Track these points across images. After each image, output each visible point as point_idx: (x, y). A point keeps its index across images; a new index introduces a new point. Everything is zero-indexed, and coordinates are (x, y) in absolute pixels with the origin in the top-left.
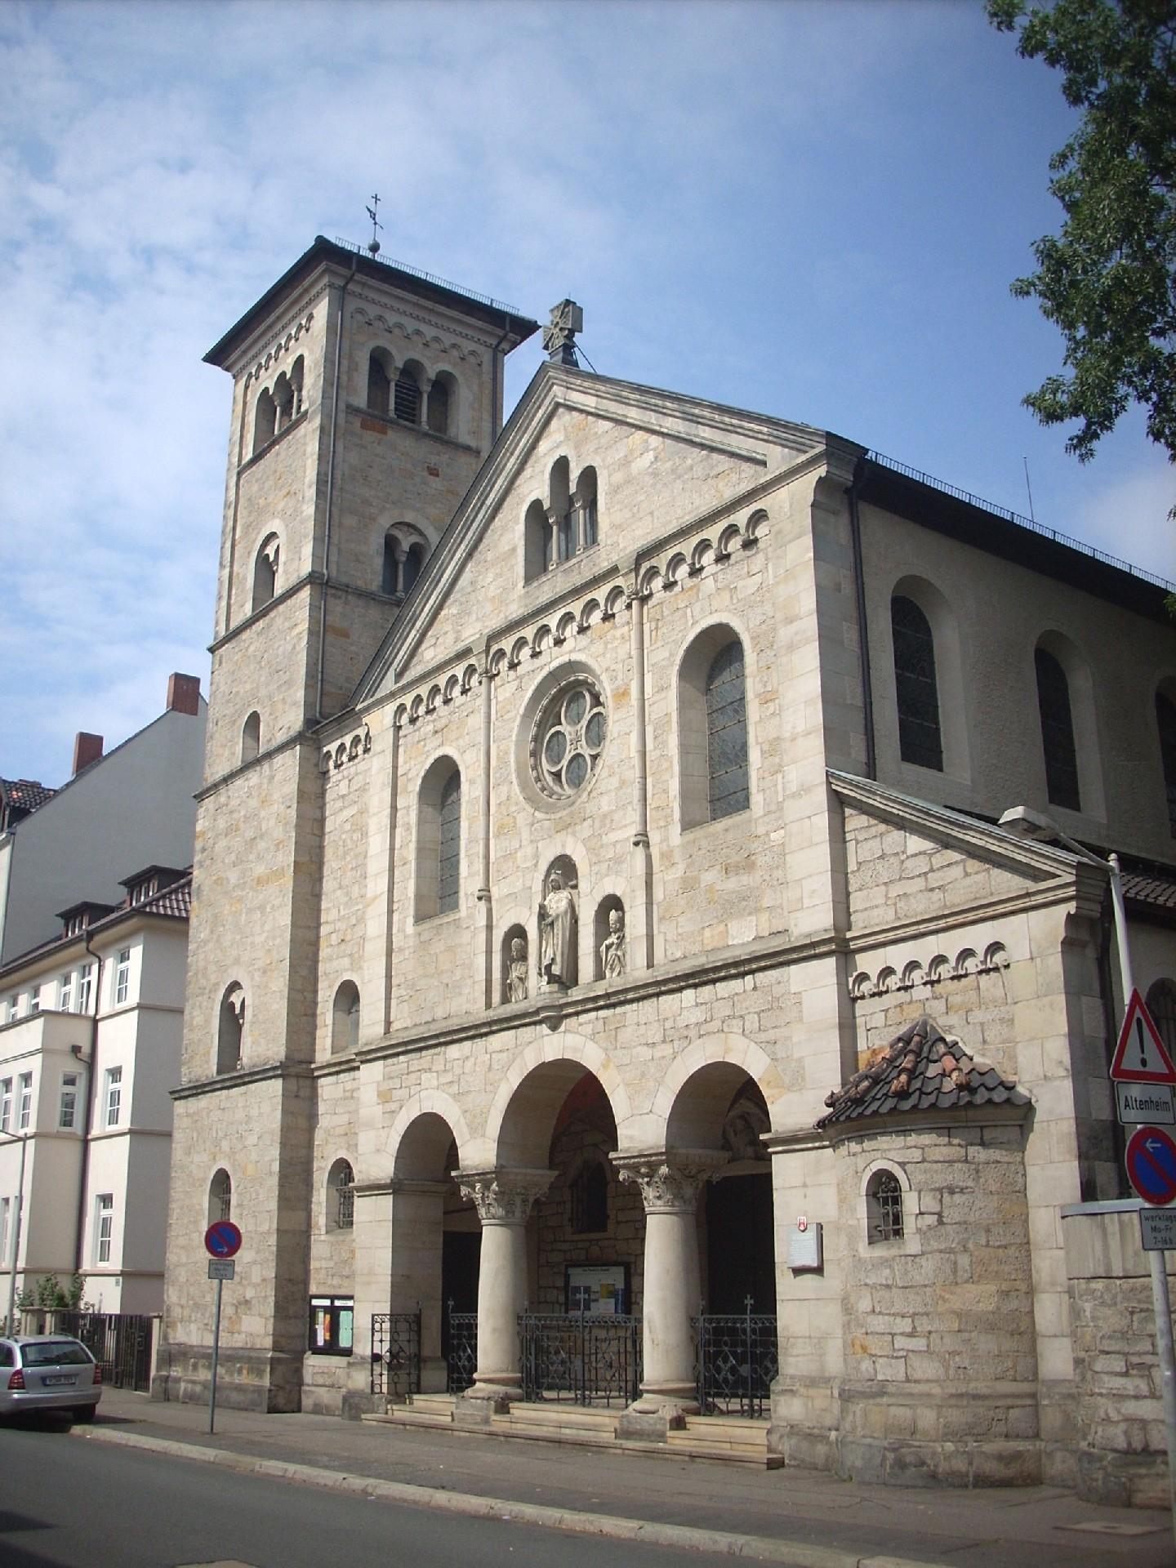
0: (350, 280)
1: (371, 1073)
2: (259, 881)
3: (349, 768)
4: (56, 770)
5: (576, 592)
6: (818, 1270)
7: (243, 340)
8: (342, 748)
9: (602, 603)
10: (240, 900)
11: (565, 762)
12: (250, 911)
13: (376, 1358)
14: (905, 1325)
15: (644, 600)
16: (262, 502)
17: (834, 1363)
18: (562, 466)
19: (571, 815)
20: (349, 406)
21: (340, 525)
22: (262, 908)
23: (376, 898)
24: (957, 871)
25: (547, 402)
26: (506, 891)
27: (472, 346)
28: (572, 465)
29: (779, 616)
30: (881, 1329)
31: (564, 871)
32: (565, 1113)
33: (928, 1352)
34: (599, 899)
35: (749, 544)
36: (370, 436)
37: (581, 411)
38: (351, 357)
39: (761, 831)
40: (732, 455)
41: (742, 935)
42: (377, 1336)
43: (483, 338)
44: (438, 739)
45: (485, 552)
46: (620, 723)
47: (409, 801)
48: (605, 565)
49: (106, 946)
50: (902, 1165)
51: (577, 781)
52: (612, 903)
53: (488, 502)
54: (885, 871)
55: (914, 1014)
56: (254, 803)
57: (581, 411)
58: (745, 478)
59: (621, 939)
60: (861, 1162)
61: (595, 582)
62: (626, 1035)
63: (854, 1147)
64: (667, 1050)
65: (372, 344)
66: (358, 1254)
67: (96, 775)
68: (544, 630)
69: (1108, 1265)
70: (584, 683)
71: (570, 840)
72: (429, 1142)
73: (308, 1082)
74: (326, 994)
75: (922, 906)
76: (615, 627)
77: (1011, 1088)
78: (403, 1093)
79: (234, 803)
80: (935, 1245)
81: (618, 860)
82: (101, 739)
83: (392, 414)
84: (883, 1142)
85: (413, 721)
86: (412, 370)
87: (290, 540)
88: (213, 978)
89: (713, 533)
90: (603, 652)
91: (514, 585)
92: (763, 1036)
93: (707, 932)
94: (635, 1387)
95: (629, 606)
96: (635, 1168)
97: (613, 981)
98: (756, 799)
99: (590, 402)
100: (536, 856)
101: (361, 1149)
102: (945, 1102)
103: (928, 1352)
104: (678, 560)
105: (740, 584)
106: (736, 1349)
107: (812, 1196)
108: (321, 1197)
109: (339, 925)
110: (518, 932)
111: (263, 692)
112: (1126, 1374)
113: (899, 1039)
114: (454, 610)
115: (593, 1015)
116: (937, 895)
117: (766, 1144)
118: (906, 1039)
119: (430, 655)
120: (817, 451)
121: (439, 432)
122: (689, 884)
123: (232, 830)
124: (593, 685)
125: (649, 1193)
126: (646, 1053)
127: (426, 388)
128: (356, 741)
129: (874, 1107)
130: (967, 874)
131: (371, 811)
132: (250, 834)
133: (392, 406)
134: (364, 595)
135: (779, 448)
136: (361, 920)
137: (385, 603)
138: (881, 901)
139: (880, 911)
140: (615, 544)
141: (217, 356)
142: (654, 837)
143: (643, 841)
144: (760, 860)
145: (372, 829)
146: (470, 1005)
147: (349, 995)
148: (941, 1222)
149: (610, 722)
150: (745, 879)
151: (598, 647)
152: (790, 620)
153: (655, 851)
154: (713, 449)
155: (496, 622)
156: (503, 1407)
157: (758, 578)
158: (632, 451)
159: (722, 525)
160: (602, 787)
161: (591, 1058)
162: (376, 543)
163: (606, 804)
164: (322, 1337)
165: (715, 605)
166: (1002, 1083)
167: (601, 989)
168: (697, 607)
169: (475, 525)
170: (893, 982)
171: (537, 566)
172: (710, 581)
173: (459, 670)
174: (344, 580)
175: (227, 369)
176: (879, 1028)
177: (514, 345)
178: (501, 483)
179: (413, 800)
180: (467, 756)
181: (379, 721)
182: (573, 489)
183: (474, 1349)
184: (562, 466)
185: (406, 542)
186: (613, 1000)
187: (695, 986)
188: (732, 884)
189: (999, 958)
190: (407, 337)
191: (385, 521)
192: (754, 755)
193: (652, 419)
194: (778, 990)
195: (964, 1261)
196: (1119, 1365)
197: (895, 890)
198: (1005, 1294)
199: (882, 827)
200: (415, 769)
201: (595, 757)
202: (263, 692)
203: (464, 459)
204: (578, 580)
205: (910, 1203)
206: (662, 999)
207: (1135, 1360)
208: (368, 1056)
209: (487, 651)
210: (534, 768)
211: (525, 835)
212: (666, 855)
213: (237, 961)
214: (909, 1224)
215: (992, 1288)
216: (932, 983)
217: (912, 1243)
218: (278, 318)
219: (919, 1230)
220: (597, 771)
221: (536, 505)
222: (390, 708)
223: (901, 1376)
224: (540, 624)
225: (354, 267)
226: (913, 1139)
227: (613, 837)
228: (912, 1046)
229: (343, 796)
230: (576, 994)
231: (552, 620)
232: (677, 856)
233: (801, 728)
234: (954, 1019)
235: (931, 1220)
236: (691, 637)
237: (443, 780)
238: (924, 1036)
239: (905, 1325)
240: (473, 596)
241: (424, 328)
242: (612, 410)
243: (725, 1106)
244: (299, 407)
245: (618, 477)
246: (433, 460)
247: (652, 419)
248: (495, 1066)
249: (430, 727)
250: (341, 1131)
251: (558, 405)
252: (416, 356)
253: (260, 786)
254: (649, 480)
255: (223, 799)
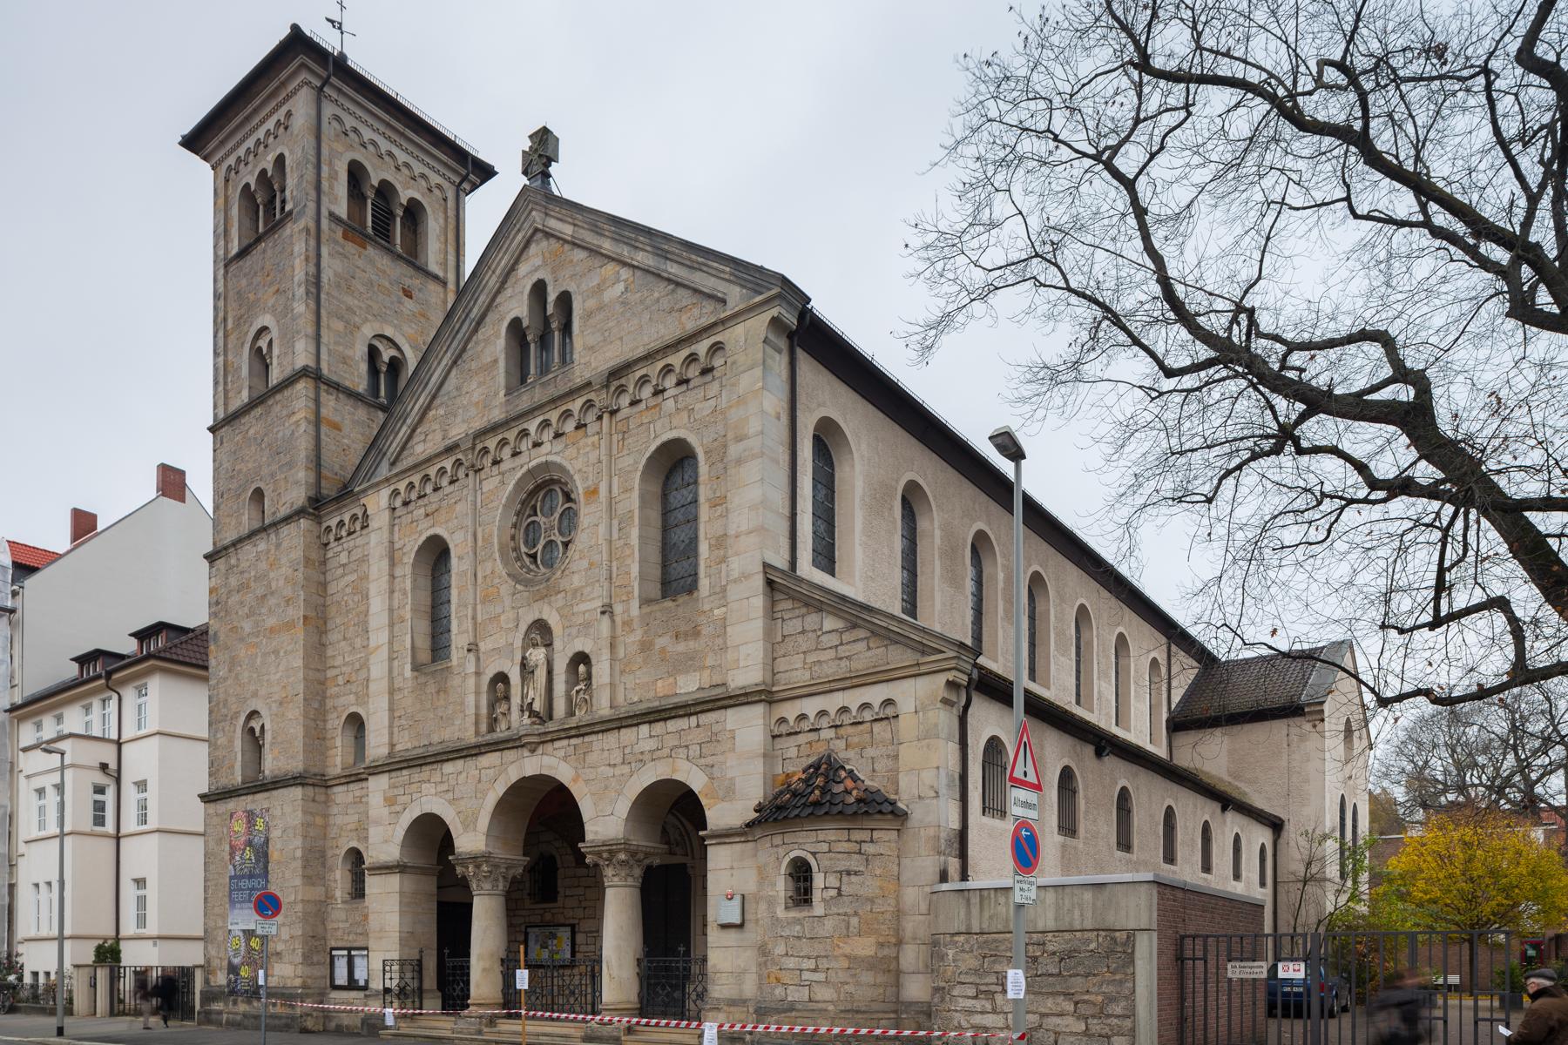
0: (326, 82)
1: (378, 785)
2: (272, 630)
3: (348, 543)
4: (57, 538)
5: (554, 402)
6: (741, 926)
7: (222, 128)
8: (341, 524)
9: (576, 413)
10: (256, 645)
11: (540, 547)
12: (265, 655)
13: (387, 991)
14: (811, 964)
15: (613, 413)
16: (251, 296)
17: (749, 989)
18: (539, 289)
19: (548, 588)
20: (331, 214)
21: (328, 327)
22: (276, 652)
23: (378, 648)
24: (861, 646)
25: (526, 225)
26: (491, 646)
27: (439, 180)
28: (550, 289)
29: (730, 435)
30: (791, 966)
31: (541, 631)
32: (545, 814)
33: (827, 982)
34: (570, 654)
35: (706, 371)
36: (351, 248)
37: (559, 238)
38: (330, 164)
39: (707, 607)
40: (696, 291)
41: (688, 686)
42: (388, 975)
43: (449, 174)
44: (430, 521)
45: (469, 363)
46: (590, 516)
47: (405, 570)
48: (578, 381)
49: (124, 682)
50: (814, 854)
51: (549, 564)
52: (582, 658)
53: (472, 316)
54: (805, 643)
55: (821, 749)
56: (263, 565)
57: (559, 238)
58: (703, 314)
59: (589, 686)
60: (781, 851)
61: (571, 394)
62: (593, 758)
63: (778, 840)
64: (626, 769)
65: (350, 156)
66: (371, 917)
67: (91, 547)
68: (426, 478)
69: (969, 926)
70: (558, 482)
71: (546, 608)
72: (431, 836)
73: (323, 790)
74: (336, 722)
75: (831, 670)
76: (586, 436)
77: (893, 803)
78: (406, 798)
79: (244, 565)
80: (835, 910)
81: (587, 625)
82: (94, 517)
83: (370, 230)
84: (802, 837)
85: (406, 504)
86: (385, 191)
87: (283, 336)
88: (234, 708)
89: (676, 359)
90: (579, 458)
91: (496, 394)
92: (703, 761)
93: (660, 684)
94: (593, 1005)
95: (600, 418)
96: (599, 854)
97: (581, 716)
98: (704, 583)
99: (567, 230)
100: (518, 620)
101: (370, 840)
102: (850, 811)
103: (827, 982)
104: (644, 380)
105: (698, 406)
106: (671, 977)
107: (733, 878)
108: (340, 878)
109: (344, 669)
110: (502, 678)
111: (265, 471)
112: (976, 997)
113: (810, 767)
114: (441, 412)
115: (565, 742)
116: (844, 663)
117: (703, 839)
118: (816, 766)
119: (420, 449)
120: (773, 292)
121: (412, 257)
122: (646, 647)
123: (243, 587)
124: (566, 484)
125: (609, 872)
126: (610, 771)
127: (400, 212)
128: (354, 518)
129: (796, 812)
130: (869, 648)
131: (372, 577)
132: (260, 592)
133: (369, 223)
134: (352, 394)
135: (738, 289)
136: (365, 665)
137: (370, 405)
138: (799, 665)
139: (799, 673)
140: (588, 364)
141: (195, 142)
142: (618, 609)
143: (607, 610)
144: (705, 631)
145: (372, 593)
146: (465, 731)
147: (356, 723)
148: (840, 894)
149: (582, 514)
150: (692, 644)
151: (572, 451)
152: (739, 439)
153: (618, 619)
154: (678, 284)
155: (478, 424)
156: (492, 1021)
157: (712, 402)
158: (604, 281)
159: (684, 353)
160: (573, 567)
161: (564, 773)
162: (361, 351)
163: (577, 581)
164: (341, 977)
165: (675, 423)
166: (887, 800)
167: (573, 722)
168: (659, 424)
169: (460, 336)
170: (805, 726)
171: (520, 375)
172: (671, 403)
173: (448, 464)
174: (335, 378)
175: (205, 158)
176: (796, 759)
177: (475, 187)
178: (483, 299)
179: (408, 570)
180: (456, 536)
181: (377, 502)
182: (550, 309)
183: (467, 983)
184: (539, 289)
185: (387, 354)
186: (583, 731)
187: (650, 722)
188: (681, 647)
189: (890, 711)
190: (381, 156)
191: (368, 331)
192: (703, 548)
193: (625, 252)
194: (716, 728)
195: (854, 921)
196: (971, 992)
197: (811, 658)
198: (881, 945)
199: (804, 610)
200: (411, 544)
201: (566, 545)
202: (265, 471)
203: (433, 287)
204: (553, 392)
205: (818, 881)
206: (623, 731)
207: (983, 988)
208: (375, 770)
209: (473, 448)
210: (515, 550)
211: (507, 601)
212: (627, 623)
213: (255, 694)
214: (817, 896)
215: (872, 940)
216: (836, 727)
217: (818, 908)
218: (256, 111)
219: (823, 900)
220: (569, 553)
221: (516, 323)
222: (385, 493)
223: (806, 998)
224: (564, 408)
225: (331, 68)
226: (821, 836)
227: (583, 607)
228: (822, 770)
229: (344, 565)
230: (551, 726)
231: (432, 471)
232: (636, 625)
233: (744, 528)
234: (851, 754)
235: (833, 893)
236: (653, 448)
237: (436, 554)
238: (829, 763)
239: (811, 964)
240: (458, 401)
241: (396, 151)
242: (588, 239)
243: (675, 812)
244: (283, 209)
245: (591, 303)
246: (408, 282)
247: (625, 252)
248: (484, 778)
249: (422, 511)
250: (352, 826)
251: (536, 230)
252: (390, 178)
253: (269, 551)
254: (619, 308)
255: (233, 561)
